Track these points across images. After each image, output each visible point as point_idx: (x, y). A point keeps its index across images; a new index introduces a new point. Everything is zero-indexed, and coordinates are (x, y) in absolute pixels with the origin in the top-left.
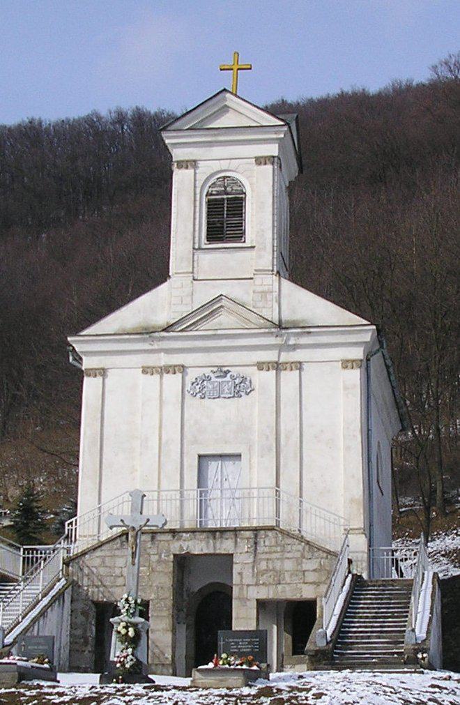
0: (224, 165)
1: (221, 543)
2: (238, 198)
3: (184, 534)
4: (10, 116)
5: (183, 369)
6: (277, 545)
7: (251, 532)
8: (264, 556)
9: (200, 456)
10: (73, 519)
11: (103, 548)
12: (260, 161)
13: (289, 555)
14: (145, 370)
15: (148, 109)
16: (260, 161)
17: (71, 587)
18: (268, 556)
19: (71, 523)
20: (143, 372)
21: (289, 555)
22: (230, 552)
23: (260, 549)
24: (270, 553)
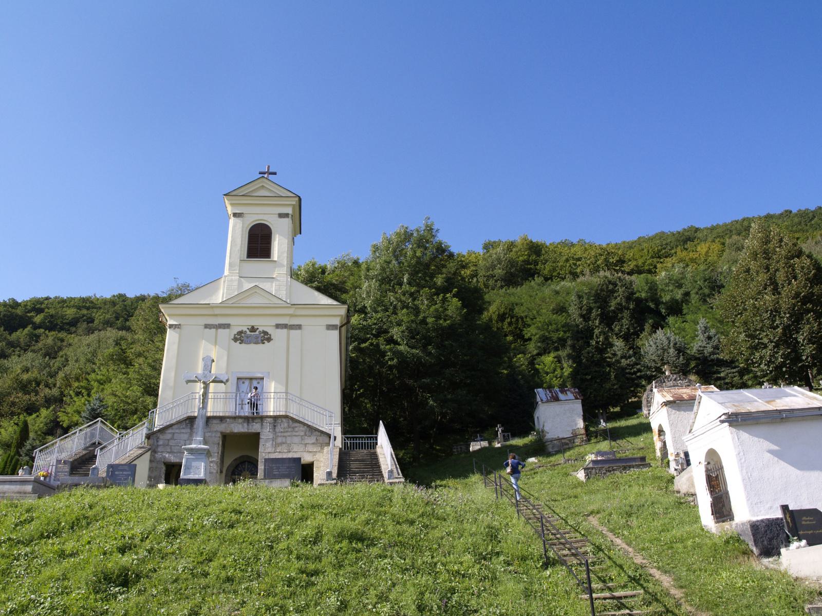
0: (261, 217)
1: (252, 426)
2: (620, 428)
3: (228, 420)
4: (814, 475)
5: (227, 326)
6: (289, 427)
7: (271, 419)
8: (279, 434)
9: (238, 379)
10: (155, 410)
11: (174, 427)
12: (281, 216)
13: (297, 434)
14: (207, 326)
15: (546, 429)
16: (281, 216)
17: (149, 453)
18: (282, 434)
19: (153, 412)
20: (374, 246)
21: (297, 434)
22: (258, 431)
23: (277, 430)
24: (284, 432)
